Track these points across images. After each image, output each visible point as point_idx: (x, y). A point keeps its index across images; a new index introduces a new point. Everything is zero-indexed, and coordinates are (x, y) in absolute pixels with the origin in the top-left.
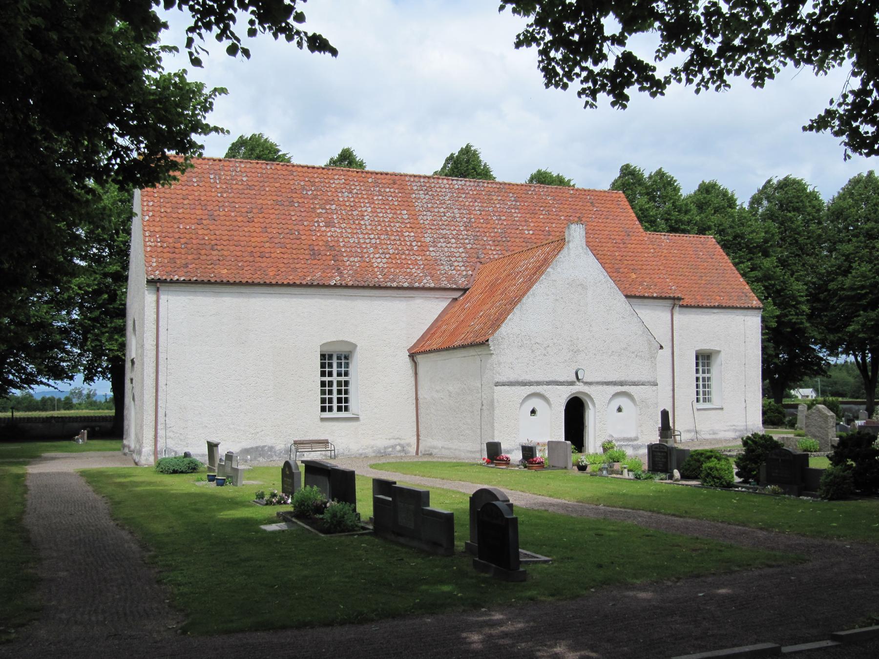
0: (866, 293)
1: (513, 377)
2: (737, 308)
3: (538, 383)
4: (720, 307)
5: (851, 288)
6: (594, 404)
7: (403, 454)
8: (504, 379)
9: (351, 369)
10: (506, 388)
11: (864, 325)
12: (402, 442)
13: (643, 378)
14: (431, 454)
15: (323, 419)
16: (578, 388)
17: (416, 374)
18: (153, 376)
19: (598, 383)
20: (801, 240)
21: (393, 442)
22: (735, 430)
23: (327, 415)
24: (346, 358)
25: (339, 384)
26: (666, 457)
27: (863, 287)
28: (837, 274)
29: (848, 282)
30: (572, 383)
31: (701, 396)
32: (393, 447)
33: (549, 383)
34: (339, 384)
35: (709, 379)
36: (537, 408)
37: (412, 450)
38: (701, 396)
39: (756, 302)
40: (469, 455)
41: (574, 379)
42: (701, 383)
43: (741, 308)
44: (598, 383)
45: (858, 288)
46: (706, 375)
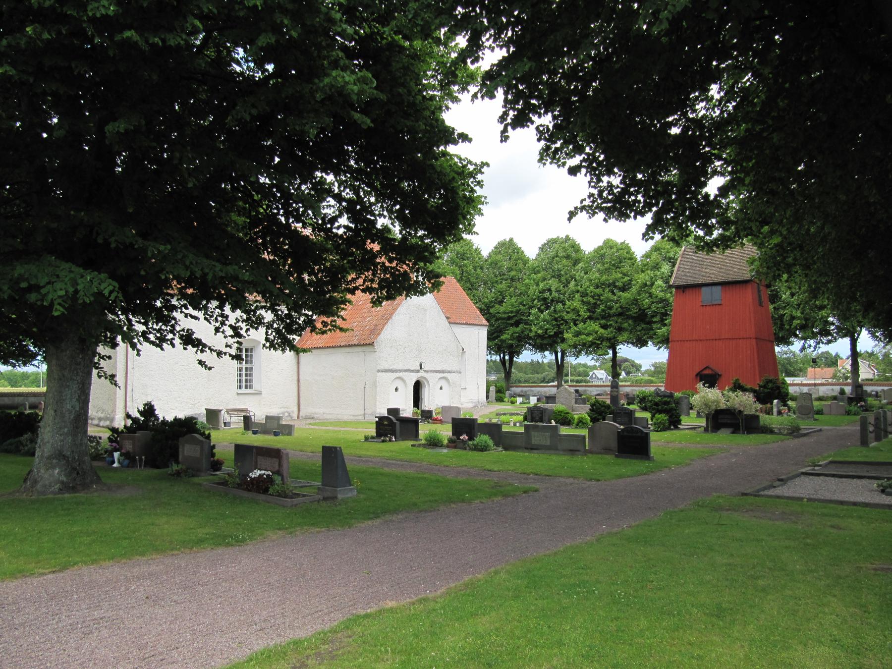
0: (514, 316)
1: (387, 367)
2: (475, 325)
3: (401, 371)
4: (466, 324)
5: (504, 313)
6: (429, 384)
7: (289, 418)
8: (382, 368)
9: (255, 359)
10: (384, 374)
11: (512, 335)
12: (288, 410)
13: (454, 369)
14: (313, 418)
15: (238, 394)
16: (422, 374)
17: (298, 363)
18: (124, 361)
19: (431, 371)
20: (472, 279)
21: (283, 410)
22: (472, 402)
23: (240, 391)
24: (252, 350)
25: (246, 369)
26: (542, 414)
27: (512, 312)
28: (495, 303)
29: (502, 309)
30: (418, 371)
31: (244, 384)
32: (283, 413)
33: (406, 371)
34: (246, 369)
35: (251, 369)
36: (399, 387)
37: (295, 415)
38: (244, 384)
39: (485, 322)
40: (352, 418)
41: (419, 368)
42: (244, 372)
43: (477, 325)
44: (431, 371)
45: (508, 313)
46: (249, 366)
